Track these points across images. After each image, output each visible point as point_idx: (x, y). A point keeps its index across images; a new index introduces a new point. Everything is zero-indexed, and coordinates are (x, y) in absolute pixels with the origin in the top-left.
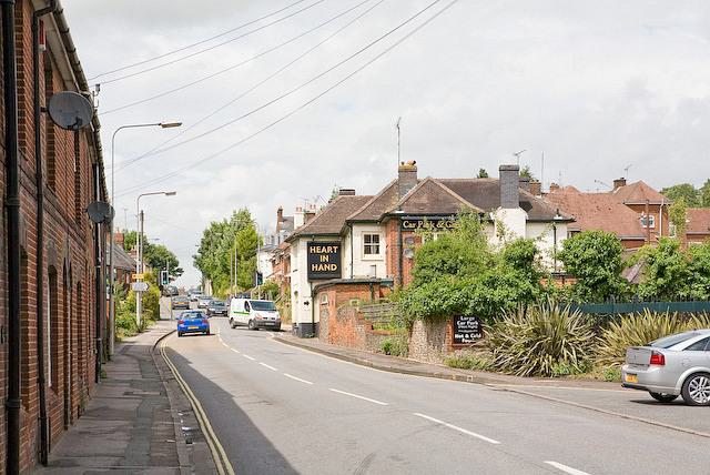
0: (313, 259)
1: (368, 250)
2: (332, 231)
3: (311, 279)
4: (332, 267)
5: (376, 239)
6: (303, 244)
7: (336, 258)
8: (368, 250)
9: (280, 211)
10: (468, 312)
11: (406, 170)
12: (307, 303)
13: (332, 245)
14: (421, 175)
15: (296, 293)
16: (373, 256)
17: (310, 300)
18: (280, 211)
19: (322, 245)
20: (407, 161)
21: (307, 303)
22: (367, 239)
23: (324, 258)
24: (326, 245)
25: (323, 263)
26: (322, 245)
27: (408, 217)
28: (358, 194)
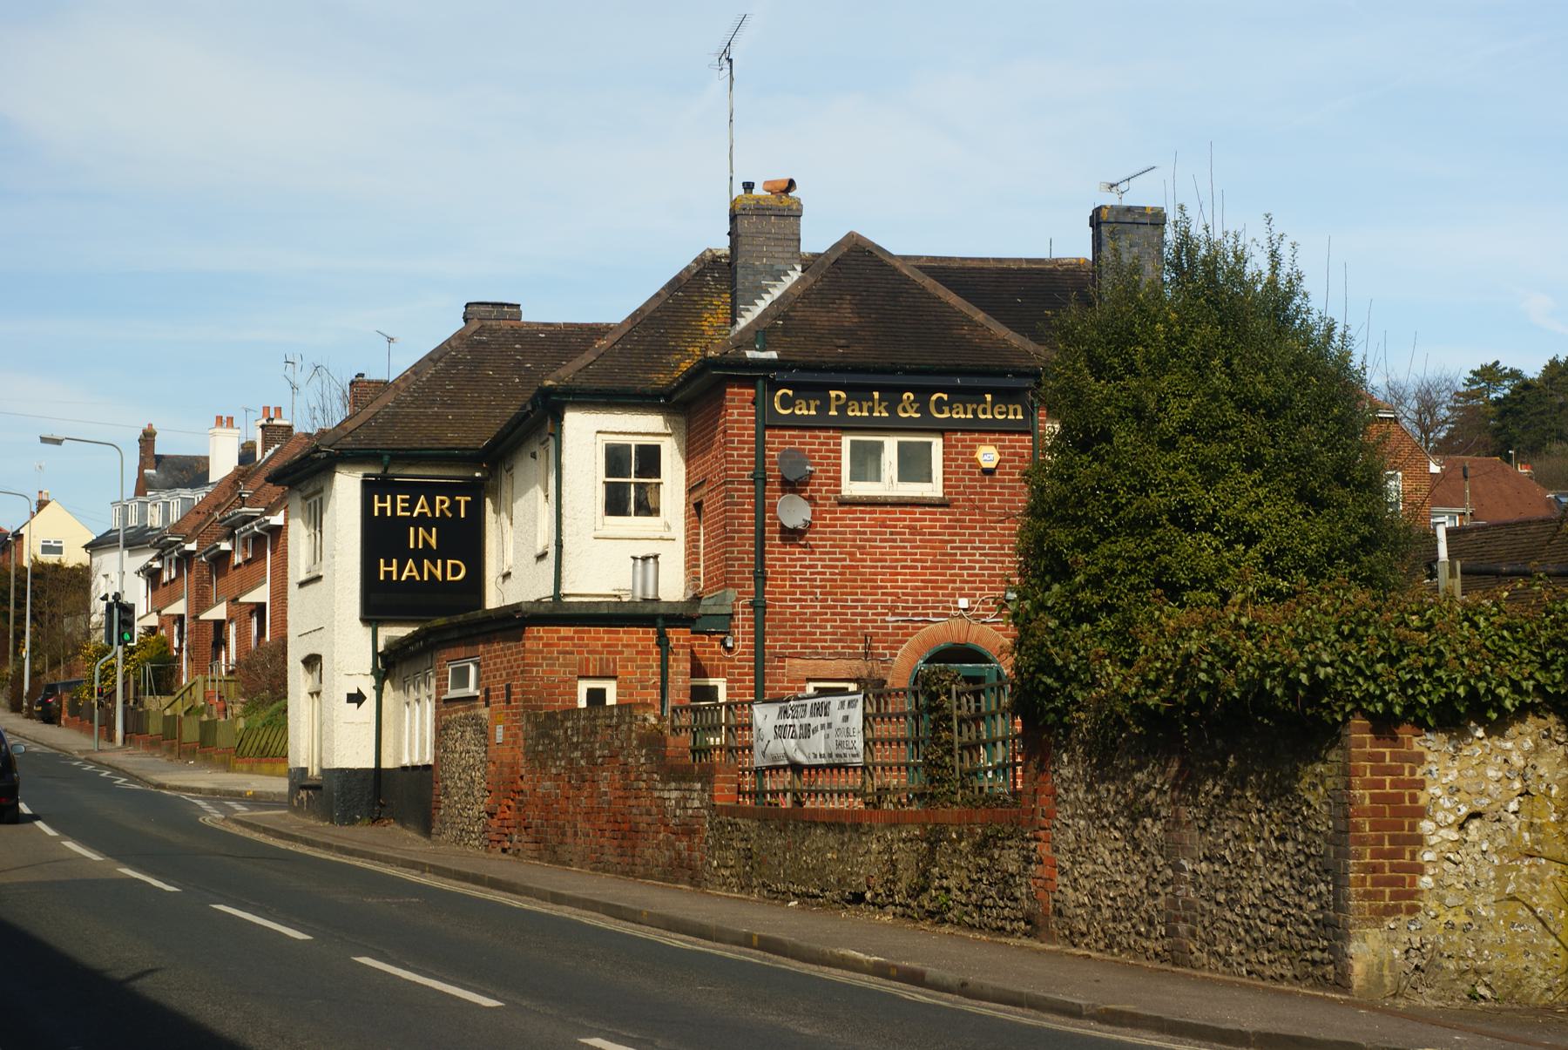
0: (380, 538)
1: (616, 504)
2: (452, 438)
3: (375, 608)
4: (452, 571)
5: (649, 459)
6: (347, 487)
7: (465, 540)
8: (616, 504)
9: (147, 438)
10: (1194, 633)
11: (760, 210)
12: (357, 698)
13: (450, 490)
14: (817, 237)
15: (312, 662)
16: (632, 524)
17: (367, 686)
18: (147, 438)
19: (414, 490)
20: (764, 172)
21: (357, 698)
22: (615, 459)
23: (416, 538)
24: (431, 490)
25: (419, 556)
26: (414, 490)
27: (795, 376)
28: (367, 377)
